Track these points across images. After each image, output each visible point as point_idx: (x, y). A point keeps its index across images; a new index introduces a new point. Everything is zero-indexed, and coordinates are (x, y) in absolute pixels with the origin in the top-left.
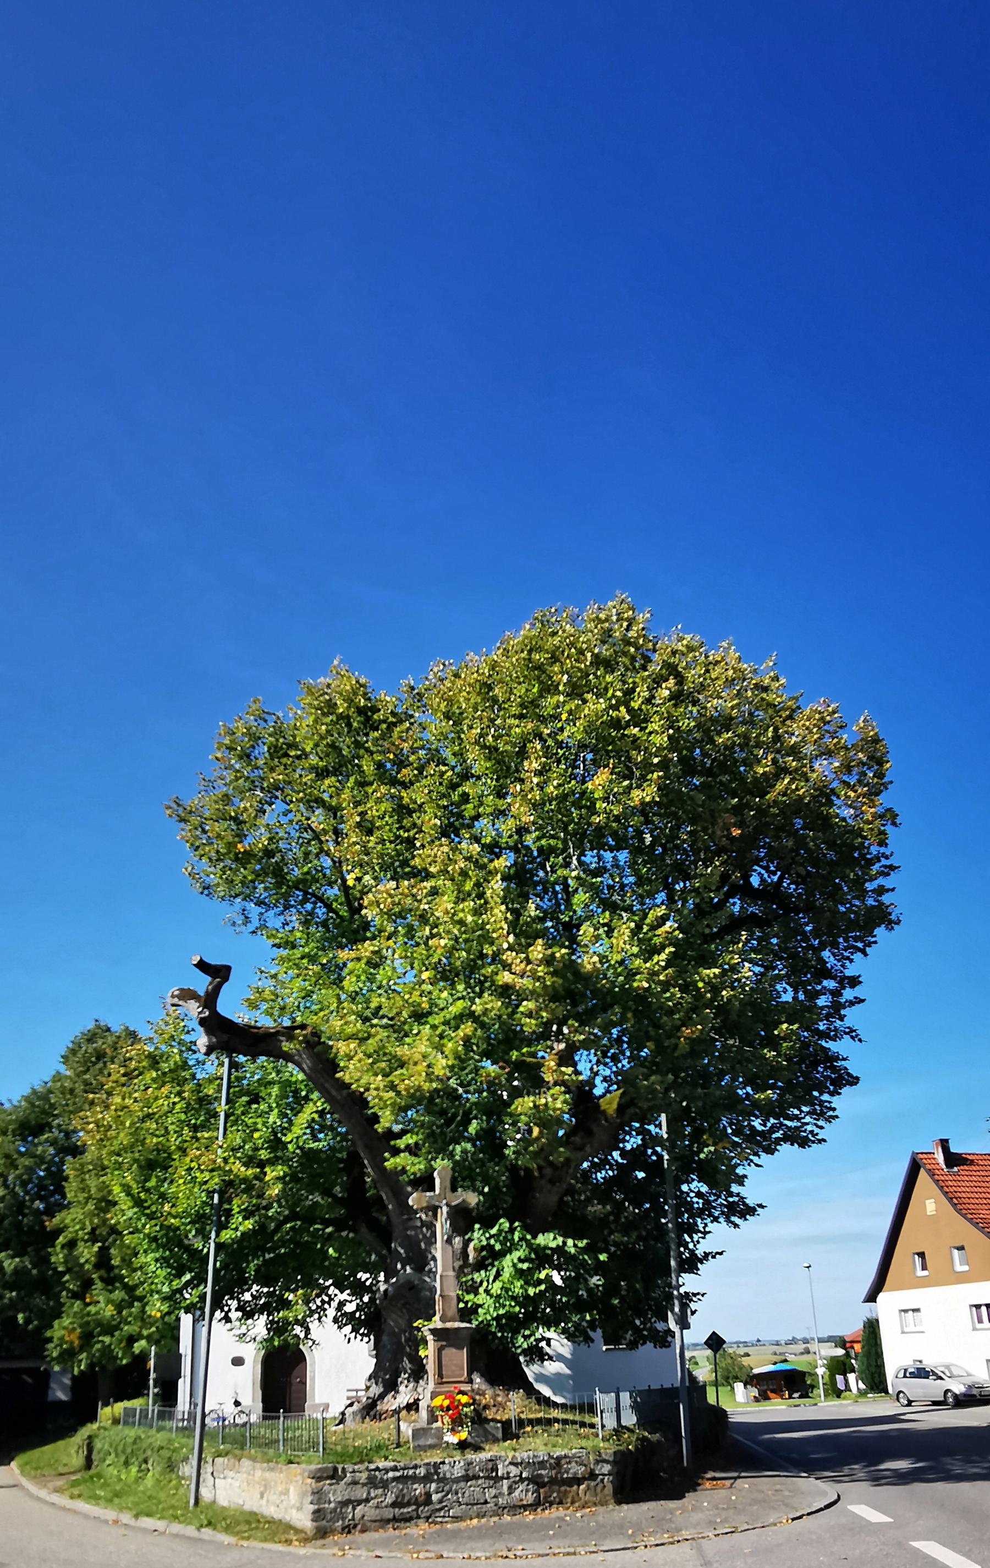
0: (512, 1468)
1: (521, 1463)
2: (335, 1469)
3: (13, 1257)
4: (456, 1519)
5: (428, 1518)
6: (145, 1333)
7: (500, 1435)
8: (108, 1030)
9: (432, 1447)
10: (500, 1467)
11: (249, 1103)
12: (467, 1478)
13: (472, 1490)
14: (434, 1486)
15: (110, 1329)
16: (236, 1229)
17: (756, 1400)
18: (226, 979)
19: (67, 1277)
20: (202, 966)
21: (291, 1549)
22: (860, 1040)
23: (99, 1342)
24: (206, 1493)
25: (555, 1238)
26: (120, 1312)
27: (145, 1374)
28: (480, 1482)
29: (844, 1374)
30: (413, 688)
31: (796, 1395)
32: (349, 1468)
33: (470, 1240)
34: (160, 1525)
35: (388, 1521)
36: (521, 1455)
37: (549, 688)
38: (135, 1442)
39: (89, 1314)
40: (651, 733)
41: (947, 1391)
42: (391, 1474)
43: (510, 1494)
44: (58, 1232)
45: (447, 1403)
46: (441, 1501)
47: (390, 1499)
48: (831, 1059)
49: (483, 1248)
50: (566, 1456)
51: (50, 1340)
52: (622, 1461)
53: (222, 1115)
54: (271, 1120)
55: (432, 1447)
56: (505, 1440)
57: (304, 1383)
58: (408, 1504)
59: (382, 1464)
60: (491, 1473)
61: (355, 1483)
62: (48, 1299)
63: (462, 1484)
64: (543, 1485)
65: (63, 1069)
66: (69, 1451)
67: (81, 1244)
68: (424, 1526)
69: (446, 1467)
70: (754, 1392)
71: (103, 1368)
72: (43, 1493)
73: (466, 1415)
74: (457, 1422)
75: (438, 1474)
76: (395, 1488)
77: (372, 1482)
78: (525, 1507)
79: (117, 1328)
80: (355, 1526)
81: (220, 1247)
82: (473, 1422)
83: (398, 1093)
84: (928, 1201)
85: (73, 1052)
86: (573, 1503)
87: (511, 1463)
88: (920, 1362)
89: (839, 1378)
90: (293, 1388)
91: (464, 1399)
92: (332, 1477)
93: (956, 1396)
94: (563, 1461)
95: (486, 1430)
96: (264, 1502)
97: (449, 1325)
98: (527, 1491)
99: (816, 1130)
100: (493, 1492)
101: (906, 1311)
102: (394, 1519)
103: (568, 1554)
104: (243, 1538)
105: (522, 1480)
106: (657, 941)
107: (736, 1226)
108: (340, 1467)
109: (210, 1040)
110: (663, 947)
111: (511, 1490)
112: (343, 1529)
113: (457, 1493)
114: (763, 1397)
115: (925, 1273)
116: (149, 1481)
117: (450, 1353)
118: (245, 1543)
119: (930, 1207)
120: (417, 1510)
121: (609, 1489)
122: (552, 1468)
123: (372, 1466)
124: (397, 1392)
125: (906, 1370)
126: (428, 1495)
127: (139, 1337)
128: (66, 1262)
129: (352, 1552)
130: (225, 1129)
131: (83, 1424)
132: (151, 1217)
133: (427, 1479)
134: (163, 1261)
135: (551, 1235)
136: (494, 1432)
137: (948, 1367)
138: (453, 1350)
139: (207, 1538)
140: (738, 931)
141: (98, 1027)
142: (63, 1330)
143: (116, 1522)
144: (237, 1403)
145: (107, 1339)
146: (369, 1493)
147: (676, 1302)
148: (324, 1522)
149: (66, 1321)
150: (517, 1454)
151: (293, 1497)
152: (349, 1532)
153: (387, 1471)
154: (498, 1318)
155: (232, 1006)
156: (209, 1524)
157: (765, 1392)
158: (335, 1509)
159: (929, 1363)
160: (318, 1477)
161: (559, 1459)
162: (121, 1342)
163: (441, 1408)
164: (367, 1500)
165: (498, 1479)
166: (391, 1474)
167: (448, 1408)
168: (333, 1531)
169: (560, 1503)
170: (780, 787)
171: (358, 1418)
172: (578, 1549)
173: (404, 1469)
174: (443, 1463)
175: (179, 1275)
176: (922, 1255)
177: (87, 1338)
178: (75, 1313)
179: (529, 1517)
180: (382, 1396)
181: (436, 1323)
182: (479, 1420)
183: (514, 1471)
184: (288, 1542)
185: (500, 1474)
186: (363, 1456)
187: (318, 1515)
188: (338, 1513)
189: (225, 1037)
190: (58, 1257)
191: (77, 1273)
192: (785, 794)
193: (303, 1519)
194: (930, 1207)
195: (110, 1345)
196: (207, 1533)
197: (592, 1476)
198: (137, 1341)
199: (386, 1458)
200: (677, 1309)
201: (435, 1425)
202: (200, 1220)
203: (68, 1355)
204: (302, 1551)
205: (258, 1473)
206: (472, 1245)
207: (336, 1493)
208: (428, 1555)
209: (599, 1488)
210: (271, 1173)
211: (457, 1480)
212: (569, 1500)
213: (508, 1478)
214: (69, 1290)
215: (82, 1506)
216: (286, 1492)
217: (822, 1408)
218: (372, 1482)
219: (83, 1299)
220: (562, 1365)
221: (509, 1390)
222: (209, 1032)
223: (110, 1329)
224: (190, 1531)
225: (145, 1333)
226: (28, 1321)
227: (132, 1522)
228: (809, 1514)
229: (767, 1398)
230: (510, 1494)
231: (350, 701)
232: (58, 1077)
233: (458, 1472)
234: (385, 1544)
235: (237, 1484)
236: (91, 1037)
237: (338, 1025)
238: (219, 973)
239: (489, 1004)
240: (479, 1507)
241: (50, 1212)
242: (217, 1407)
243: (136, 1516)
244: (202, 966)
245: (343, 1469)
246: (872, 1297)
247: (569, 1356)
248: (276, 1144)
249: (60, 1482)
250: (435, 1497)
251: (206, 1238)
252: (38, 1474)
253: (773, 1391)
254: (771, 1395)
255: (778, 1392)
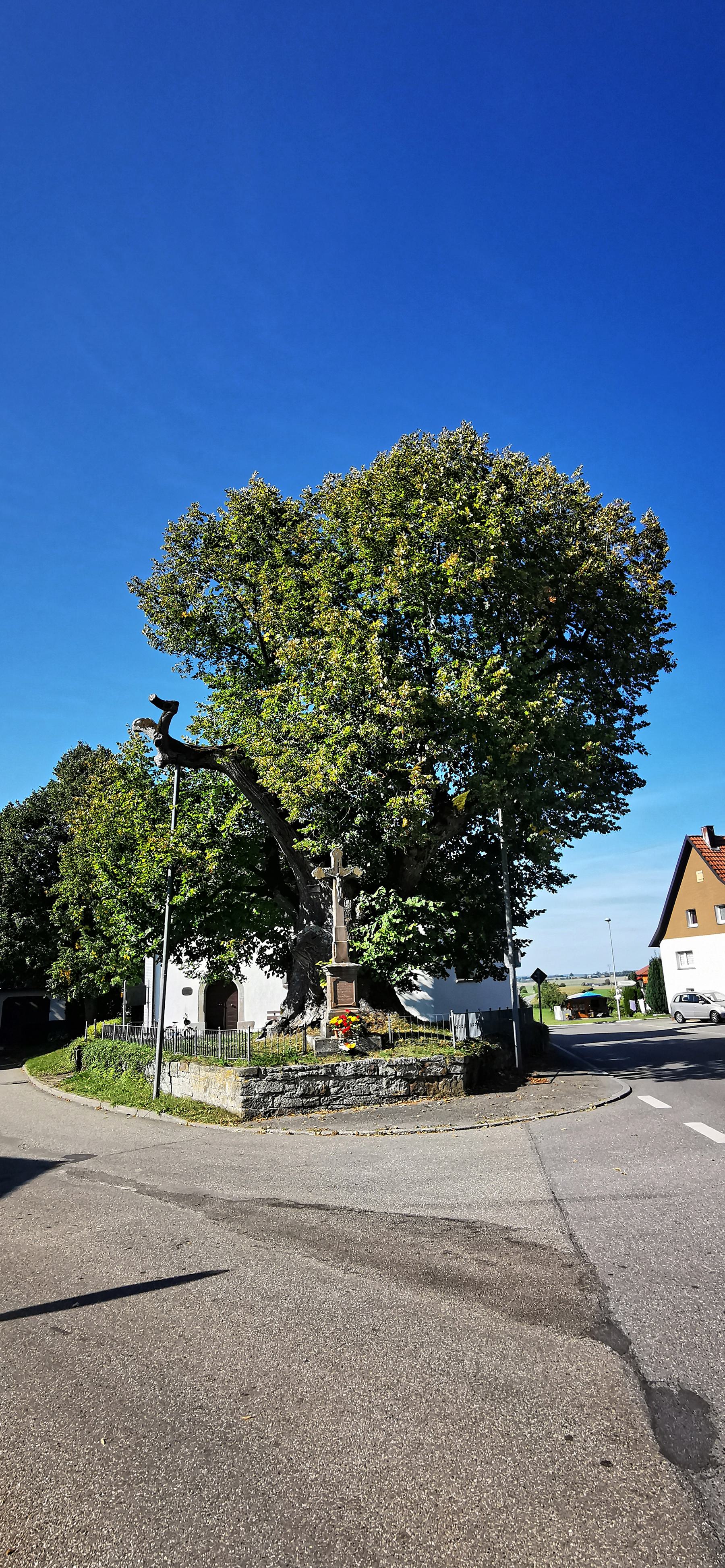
0: (389, 1068)
1: (396, 1065)
2: (259, 1070)
3: (21, 916)
4: (349, 1106)
5: (328, 1105)
6: (119, 971)
7: (380, 1045)
8: (89, 749)
9: (330, 1053)
10: (380, 1068)
11: (193, 803)
12: (356, 1076)
13: (360, 1084)
14: (331, 1082)
15: (93, 969)
16: (185, 895)
17: (570, 1018)
18: (175, 711)
19: (61, 931)
20: (157, 702)
21: (227, 1128)
22: (646, 753)
23: (85, 978)
24: (165, 1088)
25: (419, 901)
26: (100, 956)
27: (123, 1002)
28: (366, 1079)
29: (635, 999)
30: (311, 495)
31: (600, 1015)
32: (269, 1069)
33: (357, 902)
34: (132, 1111)
35: (299, 1107)
36: (396, 1060)
37: (412, 494)
38: (112, 1051)
39: (77, 957)
40: (488, 527)
41: (712, 1012)
42: (300, 1074)
43: (388, 1088)
44: (54, 898)
45: (340, 1021)
46: (337, 1093)
47: (299, 1091)
48: (625, 767)
49: (367, 908)
50: (429, 1060)
51: (50, 976)
52: (470, 1063)
53: (173, 811)
54: (209, 815)
55: (330, 1053)
56: (384, 1048)
57: (235, 1007)
58: (313, 1095)
59: (293, 1066)
60: (374, 1073)
61: (274, 1080)
62: (48, 947)
63: (353, 1081)
64: (412, 1081)
65: (55, 778)
66: (65, 1057)
67: (71, 906)
68: (324, 1110)
69: (341, 1069)
70: (569, 1012)
71: (88, 996)
72: (46, 1088)
73: (355, 1031)
74: (348, 1036)
75: (335, 1074)
76: (303, 1084)
77: (286, 1080)
78: (399, 1097)
79: (98, 967)
80: (274, 1112)
81: (172, 908)
82: (360, 1036)
83: (303, 794)
84: (698, 872)
85: (63, 766)
86: (434, 1094)
87: (388, 1066)
88: (692, 990)
89: (632, 1003)
90: (228, 1011)
91: (353, 1019)
92: (256, 1076)
93: (719, 1015)
94: (427, 1064)
95: (370, 1041)
96: (207, 1094)
97: (342, 964)
98: (400, 1085)
99: (614, 821)
100: (375, 1086)
101: (681, 953)
102: (303, 1106)
103: (431, 1132)
104: (192, 1120)
105: (396, 1078)
106: (494, 681)
107: (554, 891)
108: (262, 1068)
109: (163, 756)
110: (498, 686)
111: (389, 1084)
112: (265, 1113)
113: (348, 1087)
114: (575, 1016)
115: (696, 925)
116: (123, 1079)
117: (342, 984)
118: (193, 1124)
119: (700, 876)
120: (319, 1100)
121: (461, 1084)
122: (419, 1068)
123: (286, 1068)
124: (304, 1014)
125: (681, 996)
126: (328, 1089)
127: (115, 974)
128: (60, 920)
129: (272, 1130)
130: (176, 822)
131: (75, 1038)
132: (122, 886)
133: (326, 1077)
134: (131, 919)
135: (417, 899)
136: (376, 1042)
137: (713, 994)
138: (346, 983)
139: (166, 1120)
140: (554, 674)
141: (82, 747)
142: (58, 969)
143: (99, 1108)
144: (187, 1022)
145: (91, 976)
146: (284, 1087)
147: (510, 948)
148: (251, 1109)
149: (61, 963)
150: (393, 1059)
151: (229, 1091)
152: (270, 1116)
153: (297, 1071)
154: (378, 959)
155: (180, 732)
156: (167, 1110)
157: (577, 1012)
158: (259, 1099)
159: (698, 991)
160: (246, 1076)
161: (423, 1062)
162: (101, 977)
163: (337, 1025)
164: (282, 1093)
165: (379, 1077)
166: (300, 1074)
167: (342, 1026)
168: (258, 1115)
169: (425, 1094)
170: (585, 566)
171: (276, 1033)
172: (439, 1128)
173: (309, 1070)
174: (338, 1065)
175: (143, 929)
176: (693, 912)
177: (77, 975)
178: (68, 957)
179: (402, 1105)
180: (293, 1017)
181: (332, 963)
182: (365, 1033)
183: (390, 1071)
184: (226, 1123)
185: (380, 1073)
186: (279, 1060)
187: (246, 1103)
188: (261, 1102)
189: (175, 755)
190: (54, 916)
191: (68, 927)
192: (589, 571)
193: (236, 1106)
194: (700, 876)
195: (93, 980)
196: (166, 1116)
197: (448, 1074)
198: (113, 977)
199: (296, 1062)
200: (510, 952)
201: (332, 1038)
202: (157, 888)
203: (63, 988)
204: (235, 1130)
205: (203, 1073)
206: (358, 906)
207: (261, 1087)
208: (328, 1132)
209: (453, 1084)
210: (210, 854)
211: (348, 1078)
212: (431, 1092)
213: (386, 1076)
214: (62, 940)
215: (73, 1096)
216: (223, 1087)
217: (620, 1024)
218: (286, 1080)
219: (73, 947)
220: (426, 994)
221: (386, 1012)
222: (162, 751)
223: (93, 969)
224: (154, 1115)
225: (119, 971)
226: (33, 963)
227: (111, 1108)
228: (609, 1102)
229: (579, 1017)
230: (388, 1088)
231: (264, 505)
232: (52, 784)
233: (349, 1071)
234: (296, 1124)
235: (188, 1081)
236: (76, 755)
237: (257, 744)
238: (170, 708)
239: (369, 728)
240: (365, 1099)
241: (48, 883)
242: (172, 1025)
243: (114, 1104)
244: (157, 702)
245: (265, 1070)
246: (656, 943)
247: (431, 987)
248: (213, 832)
249: (58, 1080)
250: (332, 1090)
251: (162, 902)
252: (43, 1073)
253: (582, 1012)
254: (582, 1015)
255: (586, 1012)
